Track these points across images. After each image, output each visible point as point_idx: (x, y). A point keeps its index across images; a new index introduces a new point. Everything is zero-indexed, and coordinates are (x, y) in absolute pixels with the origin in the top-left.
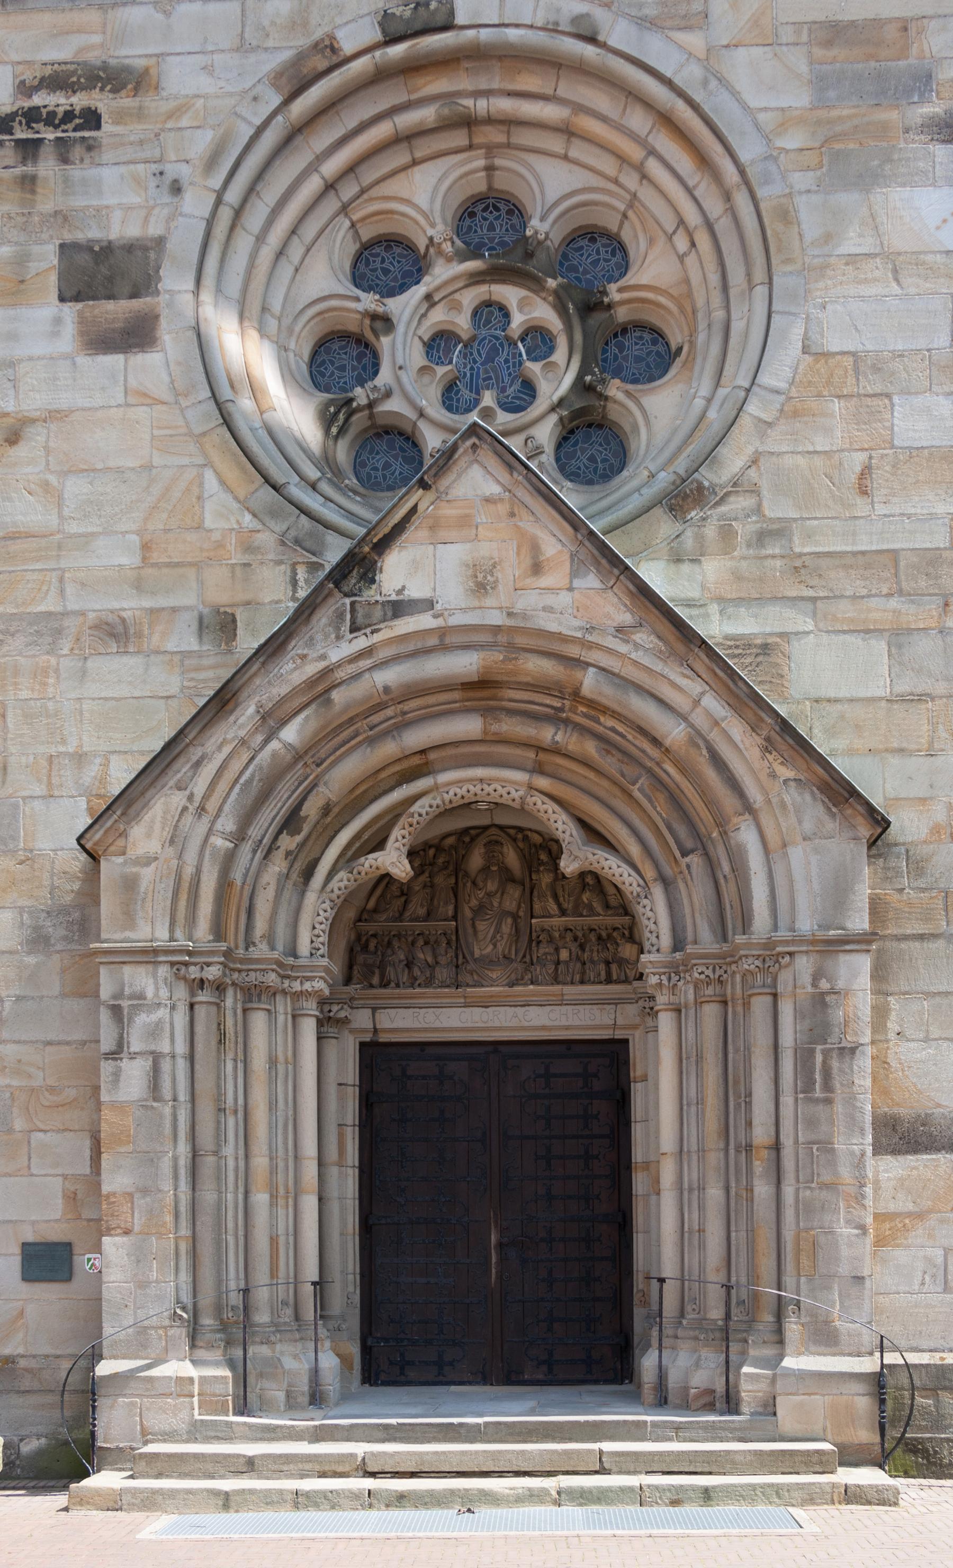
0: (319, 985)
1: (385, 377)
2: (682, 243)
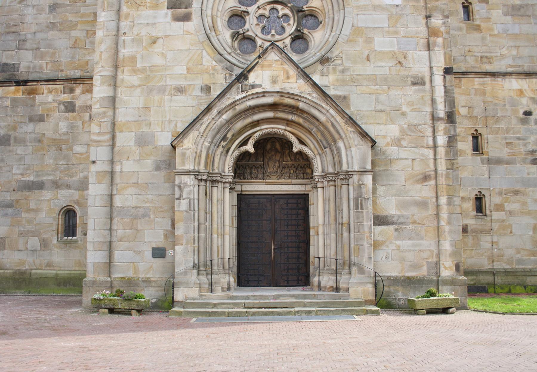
0: (230, 180)
1: (247, 26)
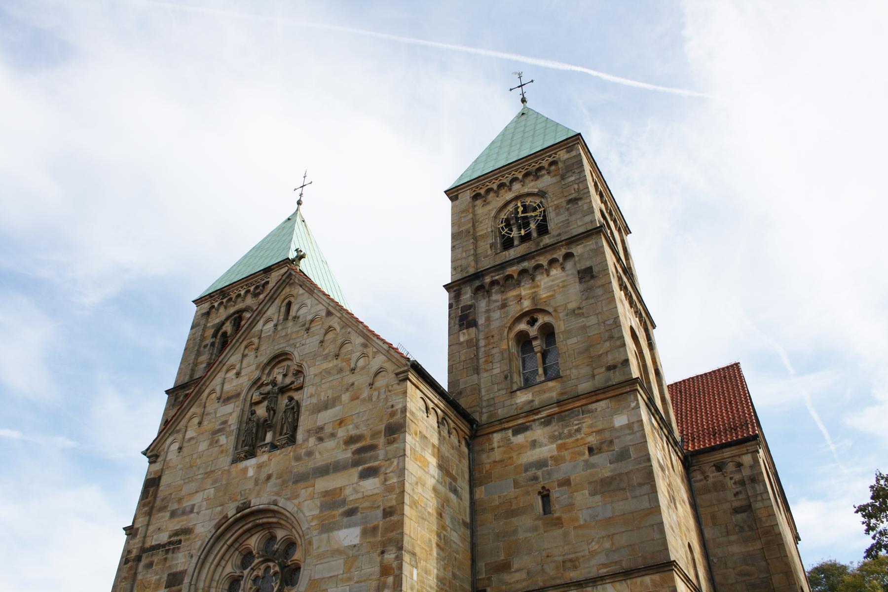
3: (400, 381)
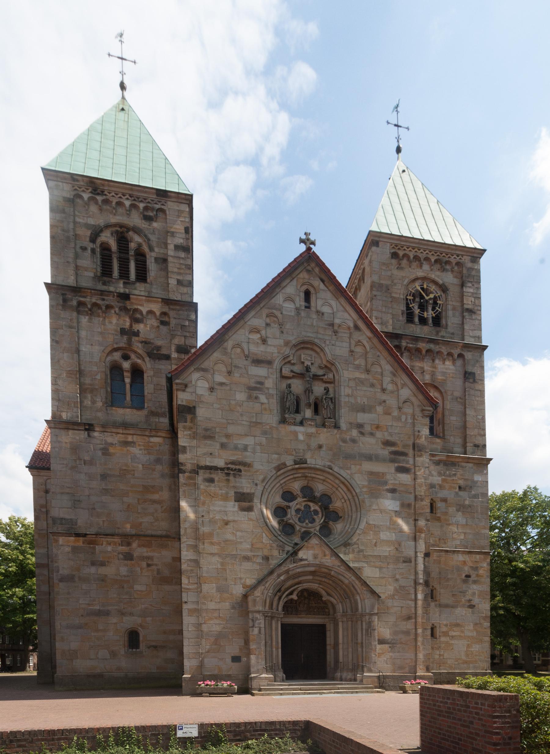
2: (343, 501)
3: (424, 415)
